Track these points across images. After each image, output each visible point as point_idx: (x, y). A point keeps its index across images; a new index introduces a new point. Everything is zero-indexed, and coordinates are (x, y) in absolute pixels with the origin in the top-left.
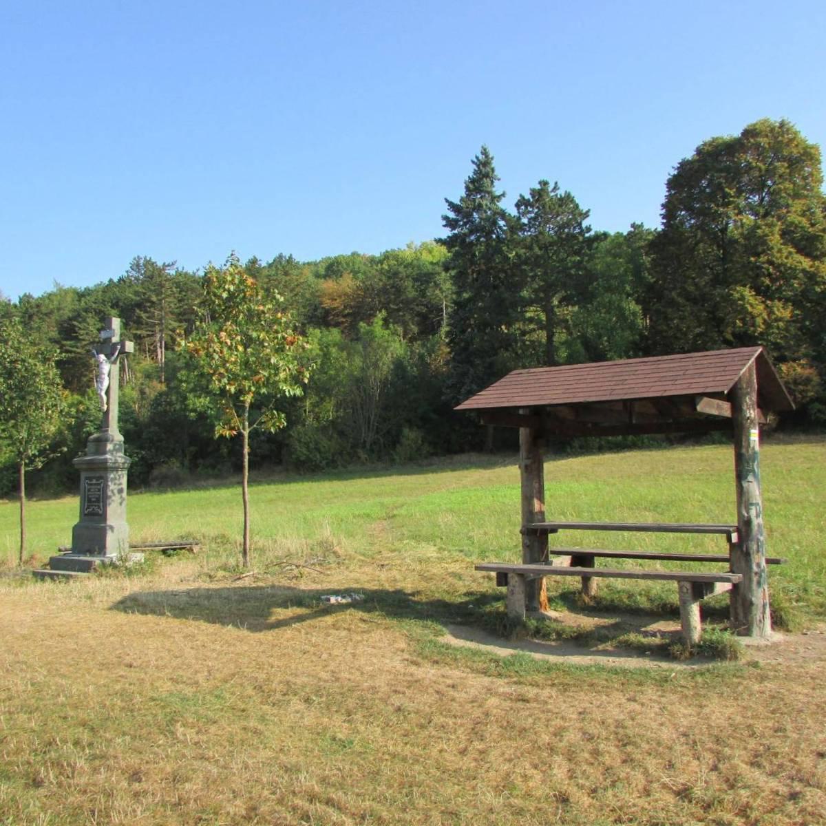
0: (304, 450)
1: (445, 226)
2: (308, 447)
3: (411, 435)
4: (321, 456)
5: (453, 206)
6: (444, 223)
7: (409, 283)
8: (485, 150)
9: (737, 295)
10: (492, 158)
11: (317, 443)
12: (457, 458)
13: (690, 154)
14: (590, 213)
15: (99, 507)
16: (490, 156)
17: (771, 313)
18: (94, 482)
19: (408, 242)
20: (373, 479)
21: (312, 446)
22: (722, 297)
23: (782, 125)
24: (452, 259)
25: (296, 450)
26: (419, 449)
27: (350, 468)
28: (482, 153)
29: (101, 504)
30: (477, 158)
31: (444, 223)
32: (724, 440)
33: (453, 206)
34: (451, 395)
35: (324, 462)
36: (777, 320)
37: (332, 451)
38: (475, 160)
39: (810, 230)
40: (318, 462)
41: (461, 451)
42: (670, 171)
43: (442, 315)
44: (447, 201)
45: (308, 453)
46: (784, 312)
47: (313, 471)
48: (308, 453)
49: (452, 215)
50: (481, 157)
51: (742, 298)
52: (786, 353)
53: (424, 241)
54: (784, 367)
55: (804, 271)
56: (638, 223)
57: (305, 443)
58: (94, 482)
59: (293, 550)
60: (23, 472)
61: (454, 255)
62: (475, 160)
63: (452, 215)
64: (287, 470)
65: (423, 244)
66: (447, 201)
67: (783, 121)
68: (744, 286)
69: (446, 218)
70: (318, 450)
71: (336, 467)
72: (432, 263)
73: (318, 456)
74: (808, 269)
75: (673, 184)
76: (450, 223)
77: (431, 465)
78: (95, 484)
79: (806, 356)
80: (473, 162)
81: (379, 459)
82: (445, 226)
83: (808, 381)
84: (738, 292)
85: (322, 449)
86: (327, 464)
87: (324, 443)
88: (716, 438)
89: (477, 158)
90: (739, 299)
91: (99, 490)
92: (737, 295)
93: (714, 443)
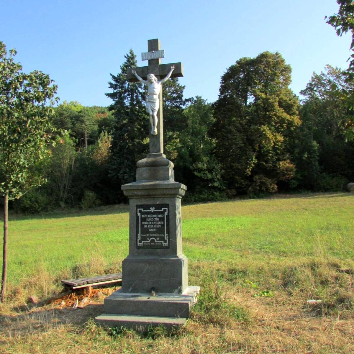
0: (29, 202)
1: (110, 87)
2: (31, 200)
3: (90, 195)
4: (39, 205)
5: (114, 77)
6: (109, 86)
7: (68, 120)
8: (132, 51)
9: (262, 129)
10: (136, 56)
11: (36, 198)
12: (116, 206)
13: (234, 63)
14: (185, 88)
15: (162, 239)
16: (135, 55)
17: (276, 138)
18: (152, 210)
19: (64, 101)
20: (76, 218)
21: (33, 199)
22: (255, 130)
23: (277, 54)
24: (115, 104)
25: (23, 201)
26: (94, 202)
27: (56, 211)
28: (130, 53)
29: (166, 235)
30: (127, 55)
31: (109, 86)
32: (255, 197)
33: (114, 77)
34: (114, 174)
35: (40, 208)
36: (278, 142)
37: (45, 202)
38: (127, 56)
39: (289, 102)
40: (37, 208)
41: (115, 203)
42: (223, 70)
43: (85, 137)
44: (111, 75)
45: (30, 203)
46: (280, 138)
47: (33, 213)
48: (30, 203)
49: (114, 82)
50: (130, 55)
51: (265, 131)
52: (280, 157)
53: (72, 101)
54: (281, 163)
55: (288, 120)
56: (199, 96)
57: (29, 198)
58: (152, 210)
59: (335, 271)
60: (7, 202)
61: (116, 102)
62: (127, 56)
63: (114, 82)
64: (17, 213)
65: (71, 102)
66: (111, 75)
67: (277, 52)
68: (265, 125)
69: (111, 84)
70: (37, 202)
71: (47, 211)
72: (77, 111)
73: (37, 205)
74: (289, 119)
75: (226, 78)
76: (112, 86)
77: (102, 210)
78: (154, 213)
79: (288, 159)
80: (125, 57)
81: (72, 207)
82: (110, 87)
83: (291, 170)
84: (262, 128)
85: (40, 201)
86: (42, 210)
87: (41, 198)
88: (252, 196)
89: (127, 55)
90: (263, 131)
91: (162, 219)
92: (262, 129)
93: (250, 198)
